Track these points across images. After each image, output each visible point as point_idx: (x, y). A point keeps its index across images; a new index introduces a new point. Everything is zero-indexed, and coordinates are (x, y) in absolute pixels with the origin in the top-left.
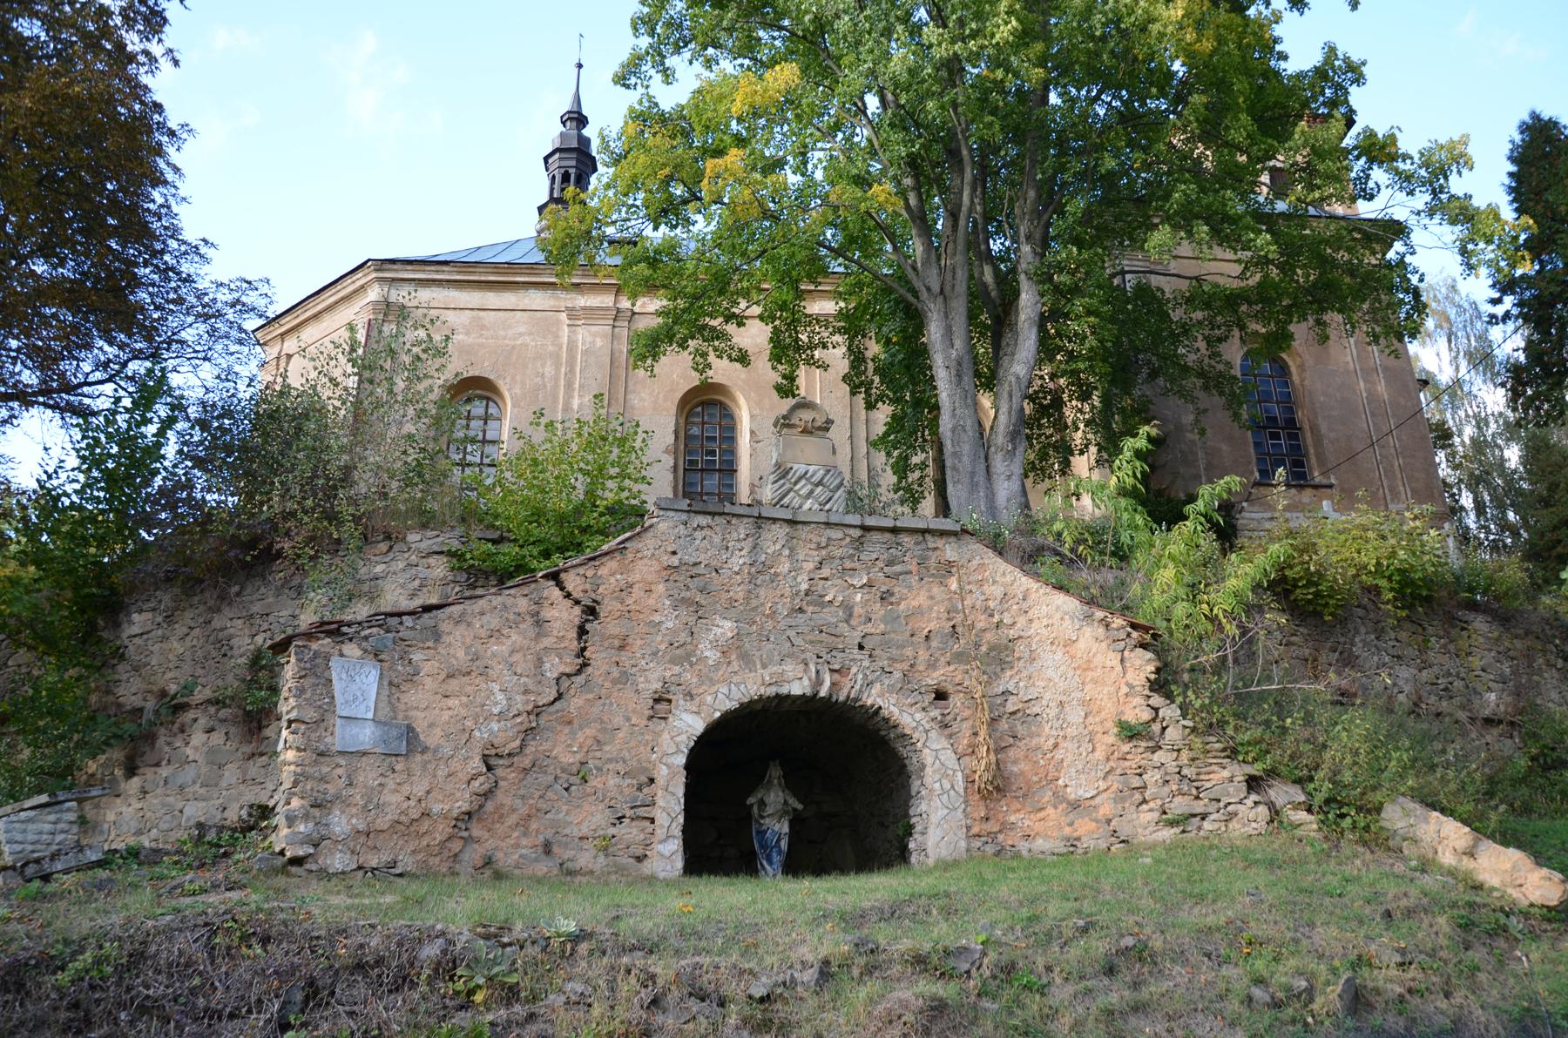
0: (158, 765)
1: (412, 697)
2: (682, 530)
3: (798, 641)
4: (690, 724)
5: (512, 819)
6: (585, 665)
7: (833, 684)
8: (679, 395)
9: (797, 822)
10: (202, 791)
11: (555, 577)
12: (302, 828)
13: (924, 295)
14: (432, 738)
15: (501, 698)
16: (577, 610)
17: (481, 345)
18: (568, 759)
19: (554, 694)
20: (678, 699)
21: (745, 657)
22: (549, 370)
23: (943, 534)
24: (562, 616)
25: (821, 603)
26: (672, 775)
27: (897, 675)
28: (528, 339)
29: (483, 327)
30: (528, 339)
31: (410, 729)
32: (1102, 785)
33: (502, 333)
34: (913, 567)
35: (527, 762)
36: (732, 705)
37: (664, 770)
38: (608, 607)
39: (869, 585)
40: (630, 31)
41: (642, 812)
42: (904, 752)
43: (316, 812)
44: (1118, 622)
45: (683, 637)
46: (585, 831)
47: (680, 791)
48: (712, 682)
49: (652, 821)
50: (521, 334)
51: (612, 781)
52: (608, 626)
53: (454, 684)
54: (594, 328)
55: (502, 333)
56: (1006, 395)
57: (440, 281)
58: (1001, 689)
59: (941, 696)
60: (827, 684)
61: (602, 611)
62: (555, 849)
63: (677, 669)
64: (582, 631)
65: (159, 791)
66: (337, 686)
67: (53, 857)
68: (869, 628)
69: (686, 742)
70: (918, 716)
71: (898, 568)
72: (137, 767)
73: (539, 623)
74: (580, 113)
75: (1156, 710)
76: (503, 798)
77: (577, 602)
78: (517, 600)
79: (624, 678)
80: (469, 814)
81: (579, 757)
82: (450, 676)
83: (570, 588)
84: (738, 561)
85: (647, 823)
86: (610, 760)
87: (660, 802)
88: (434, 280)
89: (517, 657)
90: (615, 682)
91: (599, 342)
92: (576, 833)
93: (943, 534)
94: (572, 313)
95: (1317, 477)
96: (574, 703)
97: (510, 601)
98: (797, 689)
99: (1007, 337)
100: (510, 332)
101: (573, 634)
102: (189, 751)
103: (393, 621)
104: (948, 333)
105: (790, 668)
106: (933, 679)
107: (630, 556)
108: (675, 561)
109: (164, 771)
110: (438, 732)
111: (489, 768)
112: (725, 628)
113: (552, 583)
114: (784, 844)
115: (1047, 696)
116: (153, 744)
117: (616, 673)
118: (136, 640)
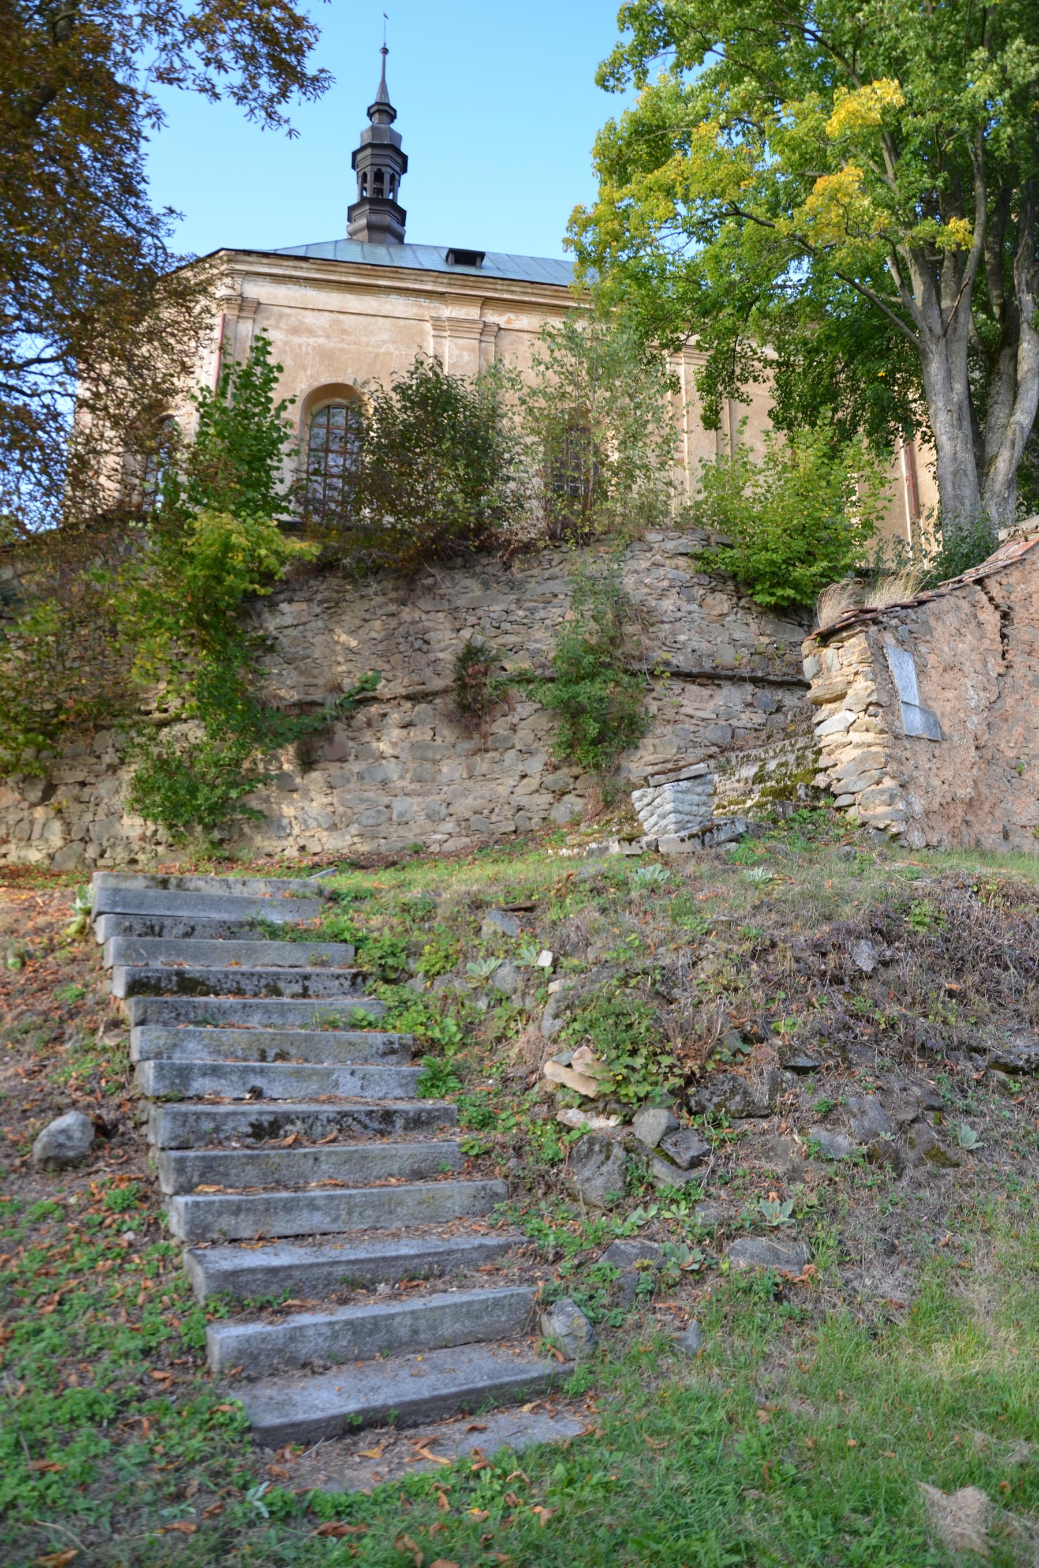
0: (343, 760)
13: (928, 335)
17: (343, 351)
28: (391, 348)
29: (344, 331)
30: (391, 348)
40: (615, 25)
50: (384, 342)
54: (460, 341)
55: (364, 339)
56: (1008, 443)
57: (298, 278)
64: (1003, 636)
65: (351, 786)
72: (316, 762)
88: (291, 277)
94: (438, 324)
100: (373, 340)
104: (949, 376)
116: (331, 741)
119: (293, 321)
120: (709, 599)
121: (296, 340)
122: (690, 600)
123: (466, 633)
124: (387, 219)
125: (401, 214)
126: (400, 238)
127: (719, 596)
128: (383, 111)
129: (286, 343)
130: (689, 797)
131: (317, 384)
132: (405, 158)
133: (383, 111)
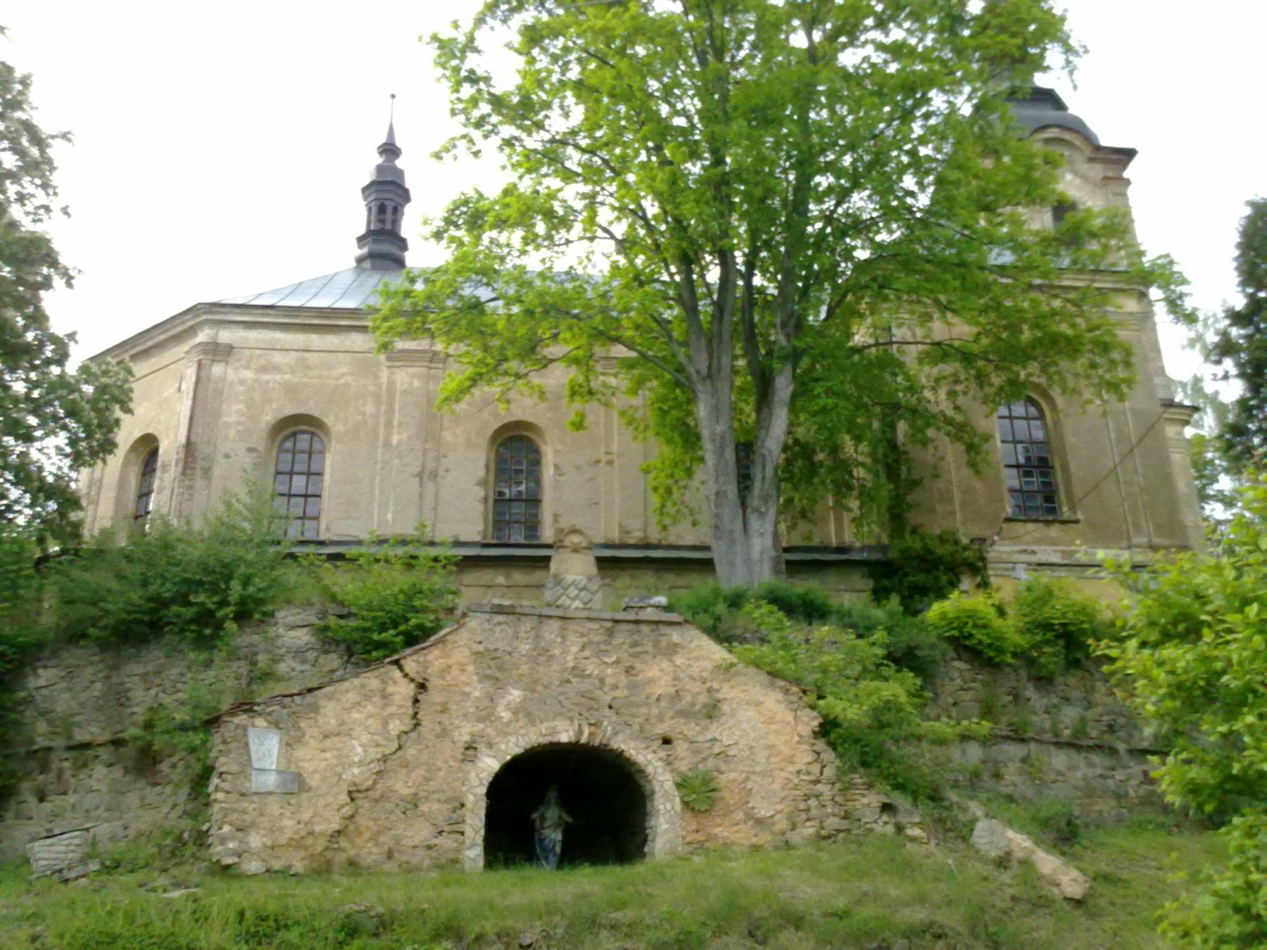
0: (64, 793)
1: (300, 753)
2: (486, 626)
3: (566, 703)
4: (490, 765)
5: (367, 835)
6: (417, 725)
7: (591, 734)
8: (490, 431)
9: (568, 832)
10: (106, 815)
11: (397, 662)
12: (231, 845)
14: (314, 781)
15: (360, 750)
16: (412, 686)
18: (405, 791)
19: (396, 746)
20: (482, 747)
21: (528, 715)
22: (370, 408)
23: (671, 624)
24: (403, 690)
25: (584, 677)
26: (477, 801)
27: (636, 727)
28: (349, 379)
29: (308, 368)
30: (349, 379)
31: (299, 775)
32: (779, 807)
33: (326, 373)
34: (649, 647)
35: (377, 794)
36: (519, 751)
37: (471, 798)
38: (434, 683)
39: (617, 662)
41: (455, 828)
42: (642, 782)
43: (239, 834)
44: (795, 689)
45: (486, 703)
46: (416, 842)
47: (482, 813)
48: (506, 734)
49: (462, 833)
50: (343, 375)
51: (435, 806)
52: (434, 696)
53: (328, 743)
54: (411, 370)
58: (710, 736)
59: (667, 741)
60: (586, 734)
61: (430, 685)
62: (396, 855)
63: (481, 726)
64: (416, 701)
66: (253, 748)
67: (70, 868)
68: (617, 693)
69: (487, 777)
70: (650, 757)
71: (638, 649)
73: (385, 696)
74: (393, 145)
75: (818, 754)
76: (362, 820)
77: (412, 680)
78: (371, 680)
79: (444, 733)
80: (339, 832)
81: (412, 790)
82: (326, 737)
83: (407, 669)
84: (524, 647)
85: (458, 836)
86: (434, 792)
87: (469, 821)
89: (371, 721)
90: (437, 736)
91: (416, 383)
92: (410, 843)
93: (671, 624)
95: (1066, 512)
96: (411, 752)
97: (366, 681)
98: (564, 738)
99: (765, 410)
101: (410, 703)
102: (93, 782)
103: (287, 700)
105: (561, 724)
106: (661, 729)
107: (449, 646)
108: (481, 648)
109: (72, 798)
110: (317, 776)
111: (352, 799)
112: (515, 695)
113: (395, 667)
114: (558, 849)
115: (742, 742)
117: (438, 728)
118: (44, 692)
119: (262, 361)
120: (321, 660)
121: (265, 377)
122: (304, 661)
123: (153, 692)
124: (386, 248)
125: (403, 244)
126: (400, 263)
127: (334, 656)
128: (390, 150)
129: (255, 381)
130: (56, 848)
131: (280, 416)
132: (406, 192)
133: (390, 150)
